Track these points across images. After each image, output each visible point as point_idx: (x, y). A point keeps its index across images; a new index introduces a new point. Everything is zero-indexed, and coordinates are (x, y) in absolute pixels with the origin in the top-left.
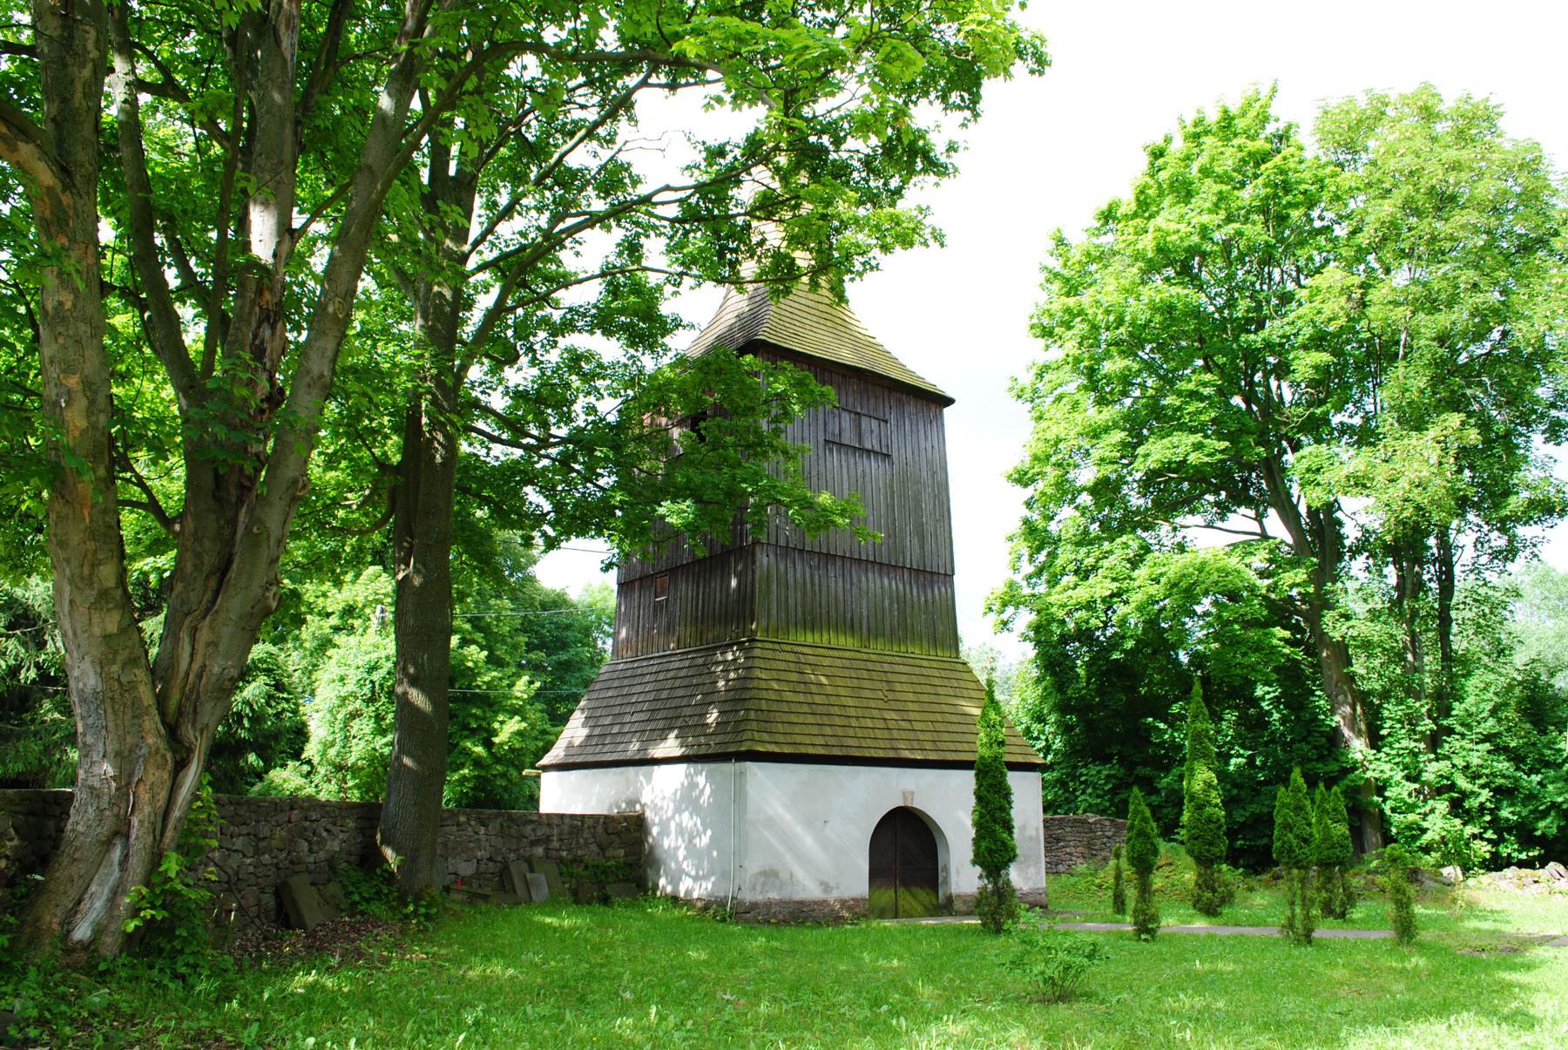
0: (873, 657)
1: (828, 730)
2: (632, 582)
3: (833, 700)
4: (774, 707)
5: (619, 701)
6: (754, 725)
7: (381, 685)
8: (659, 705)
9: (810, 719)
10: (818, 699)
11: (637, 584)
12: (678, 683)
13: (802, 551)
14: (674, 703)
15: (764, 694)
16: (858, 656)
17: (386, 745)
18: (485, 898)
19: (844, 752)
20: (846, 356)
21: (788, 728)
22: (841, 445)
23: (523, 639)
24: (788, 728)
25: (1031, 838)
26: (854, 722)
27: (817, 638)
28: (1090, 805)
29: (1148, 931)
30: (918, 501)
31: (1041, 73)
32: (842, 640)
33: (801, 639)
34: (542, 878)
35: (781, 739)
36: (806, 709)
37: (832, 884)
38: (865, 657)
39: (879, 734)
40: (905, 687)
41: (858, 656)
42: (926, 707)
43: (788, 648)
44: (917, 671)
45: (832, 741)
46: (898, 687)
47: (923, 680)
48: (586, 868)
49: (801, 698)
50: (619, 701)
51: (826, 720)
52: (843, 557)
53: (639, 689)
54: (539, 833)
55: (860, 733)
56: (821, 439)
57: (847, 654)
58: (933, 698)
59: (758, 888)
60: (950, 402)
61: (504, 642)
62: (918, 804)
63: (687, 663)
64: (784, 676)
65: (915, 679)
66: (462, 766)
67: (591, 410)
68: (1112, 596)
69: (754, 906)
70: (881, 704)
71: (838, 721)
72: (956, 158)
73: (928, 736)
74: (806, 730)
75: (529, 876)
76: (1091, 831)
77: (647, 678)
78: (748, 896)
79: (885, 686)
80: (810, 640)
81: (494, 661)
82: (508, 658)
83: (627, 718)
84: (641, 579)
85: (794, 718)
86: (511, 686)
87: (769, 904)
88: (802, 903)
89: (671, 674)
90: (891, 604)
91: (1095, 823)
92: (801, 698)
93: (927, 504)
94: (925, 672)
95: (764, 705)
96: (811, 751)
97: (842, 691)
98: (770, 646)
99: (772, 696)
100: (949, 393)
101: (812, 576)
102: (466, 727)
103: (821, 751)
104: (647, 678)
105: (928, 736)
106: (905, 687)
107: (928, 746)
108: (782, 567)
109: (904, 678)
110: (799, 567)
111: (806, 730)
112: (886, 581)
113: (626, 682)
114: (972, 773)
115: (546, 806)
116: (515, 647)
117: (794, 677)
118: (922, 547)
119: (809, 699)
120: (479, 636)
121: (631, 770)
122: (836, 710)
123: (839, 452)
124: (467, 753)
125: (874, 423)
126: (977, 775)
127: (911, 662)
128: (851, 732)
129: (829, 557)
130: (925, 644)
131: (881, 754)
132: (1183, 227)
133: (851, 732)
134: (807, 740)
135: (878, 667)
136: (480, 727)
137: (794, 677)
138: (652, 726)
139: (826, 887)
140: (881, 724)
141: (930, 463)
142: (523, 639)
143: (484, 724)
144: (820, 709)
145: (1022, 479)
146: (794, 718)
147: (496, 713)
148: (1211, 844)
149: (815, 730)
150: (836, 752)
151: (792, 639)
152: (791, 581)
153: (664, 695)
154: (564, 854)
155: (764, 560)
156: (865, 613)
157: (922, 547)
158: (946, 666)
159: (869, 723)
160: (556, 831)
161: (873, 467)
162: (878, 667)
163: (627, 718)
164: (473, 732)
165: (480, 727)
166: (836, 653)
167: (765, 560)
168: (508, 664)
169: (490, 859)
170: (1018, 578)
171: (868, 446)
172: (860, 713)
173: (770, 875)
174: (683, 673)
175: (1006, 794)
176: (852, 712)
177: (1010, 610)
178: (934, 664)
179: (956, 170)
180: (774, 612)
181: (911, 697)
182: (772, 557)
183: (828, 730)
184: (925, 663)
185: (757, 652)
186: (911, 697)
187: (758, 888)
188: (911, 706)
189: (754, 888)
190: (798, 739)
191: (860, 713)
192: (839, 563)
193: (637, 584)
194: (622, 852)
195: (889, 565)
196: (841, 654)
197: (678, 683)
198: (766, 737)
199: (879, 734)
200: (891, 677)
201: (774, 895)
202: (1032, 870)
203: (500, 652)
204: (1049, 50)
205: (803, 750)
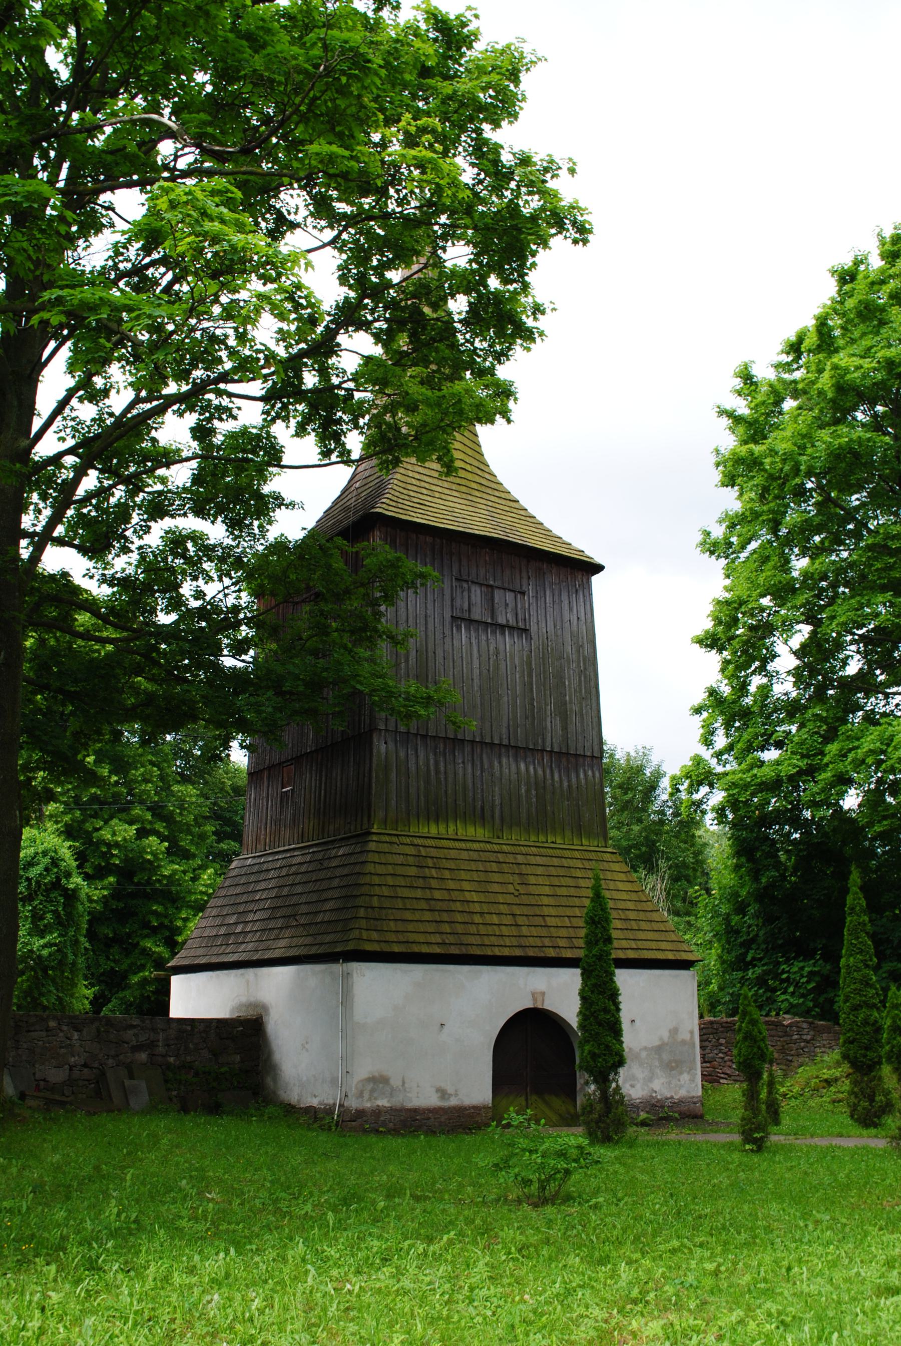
0: (505, 848)
1: (446, 928)
2: (261, 771)
3: (455, 895)
4: (387, 904)
5: (244, 898)
6: (363, 923)
7: (38, 882)
8: (279, 903)
9: (428, 916)
10: (437, 895)
11: (266, 774)
12: (298, 879)
13: (425, 737)
14: (294, 900)
15: (377, 890)
16: (488, 847)
17: (44, 946)
18: (62, 1104)
19: (464, 950)
20: (480, 526)
21: (401, 926)
22: (470, 622)
23: (209, 828)
24: (401, 926)
25: (684, 1042)
26: (477, 919)
27: (442, 829)
28: (792, 1006)
29: (755, 1141)
30: (560, 678)
31: (585, 242)
32: (471, 831)
33: (424, 831)
34: (143, 1085)
35: (392, 937)
36: (423, 904)
37: (450, 1090)
38: (496, 848)
39: (505, 930)
40: (541, 880)
41: (488, 847)
42: (564, 901)
43: (408, 840)
44: (556, 862)
45: (451, 939)
46: (532, 879)
47: (561, 872)
48: (197, 1074)
49: (419, 893)
50: (244, 898)
51: (445, 917)
52: (473, 742)
53: (263, 885)
54: (142, 1039)
55: (483, 930)
56: (448, 616)
57: (476, 846)
58: (572, 891)
59: (366, 1095)
60: (598, 568)
61: (189, 832)
62: (549, 1005)
63: (308, 858)
64: (400, 870)
65: (553, 871)
66: (142, 968)
67: (199, 594)
68: (801, 773)
69: (360, 1113)
70: (510, 899)
71: (459, 918)
72: (543, 323)
73: (563, 933)
74: (421, 927)
75: (127, 1083)
76: (786, 1034)
77: (272, 874)
78: (353, 1103)
79: (517, 879)
80: (434, 831)
81: (176, 852)
82: (193, 849)
83: (250, 917)
84: (269, 768)
85: (408, 915)
86: (194, 879)
87: (377, 1112)
88: (415, 1111)
89: (293, 869)
90: (528, 791)
91: (790, 1025)
92: (419, 893)
93: (571, 681)
94: (565, 863)
95: (375, 902)
96: (425, 949)
97: (466, 886)
98: (387, 839)
99: (386, 891)
100: (598, 559)
101: (437, 763)
102: (146, 925)
103: (437, 950)
104: (272, 874)
105: (563, 933)
106: (541, 880)
107: (562, 943)
108: (402, 754)
109: (540, 871)
110: (422, 754)
111: (421, 927)
112: (522, 766)
113: (253, 878)
114: (578, 971)
115: (177, 1010)
116: (202, 837)
117: (413, 871)
118: (565, 728)
119: (428, 894)
120: (160, 826)
121: (250, 972)
122: (458, 906)
123: (468, 629)
124: (145, 952)
125: (509, 596)
126: (582, 974)
127: (550, 852)
128: (473, 929)
129: (456, 743)
130: (568, 833)
131: (506, 952)
132: (867, 364)
133: (473, 929)
134: (421, 938)
135: (510, 858)
136: (161, 925)
137: (413, 871)
138: (272, 924)
139: (443, 1093)
140: (508, 920)
141: (575, 636)
142: (209, 828)
143: (166, 922)
144: (439, 905)
145: (710, 642)
146: (408, 915)
147: (179, 909)
148: (867, 1048)
149: (431, 928)
150: (454, 950)
151: (413, 830)
152: (413, 768)
153: (285, 891)
154: (172, 1060)
155: (381, 747)
156: (497, 802)
157: (565, 728)
158: (592, 856)
159: (495, 919)
160: (161, 1036)
161: (508, 643)
162: (510, 858)
163: (250, 917)
164: (155, 931)
165: (161, 925)
166: (463, 845)
167: (383, 747)
168: (194, 856)
169: (85, 1065)
170: (706, 754)
171: (501, 620)
172: (485, 908)
173: (378, 1081)
174: (303, 868)
175: (613, 995)
176: (477, 908)
177: (704, 790)
178: (577, 854)
179: (541, 334)
180: (393, 803)
181: (547, 890)
182: (391, 745)
183: (446, 928)
184: (568, 854)
185: (372, 846)
186: (547, 890)
187: (366, 1095)
188: (546, 900)
189: (360, 1095)
190: (412, 937)
191: (485, 908)
192: (467, 749)
193: (266, 774)
194: (238, 1058)
195: (527, 749)
196: (469, 845)
197: (298, 879)
198: (375, 935)
199: (505, 930)
200: (525, 870)
201: (383, 1102)
202: (685, 1077)
203: (185, 842)
204: (593, 219)
205: (416, 949)
